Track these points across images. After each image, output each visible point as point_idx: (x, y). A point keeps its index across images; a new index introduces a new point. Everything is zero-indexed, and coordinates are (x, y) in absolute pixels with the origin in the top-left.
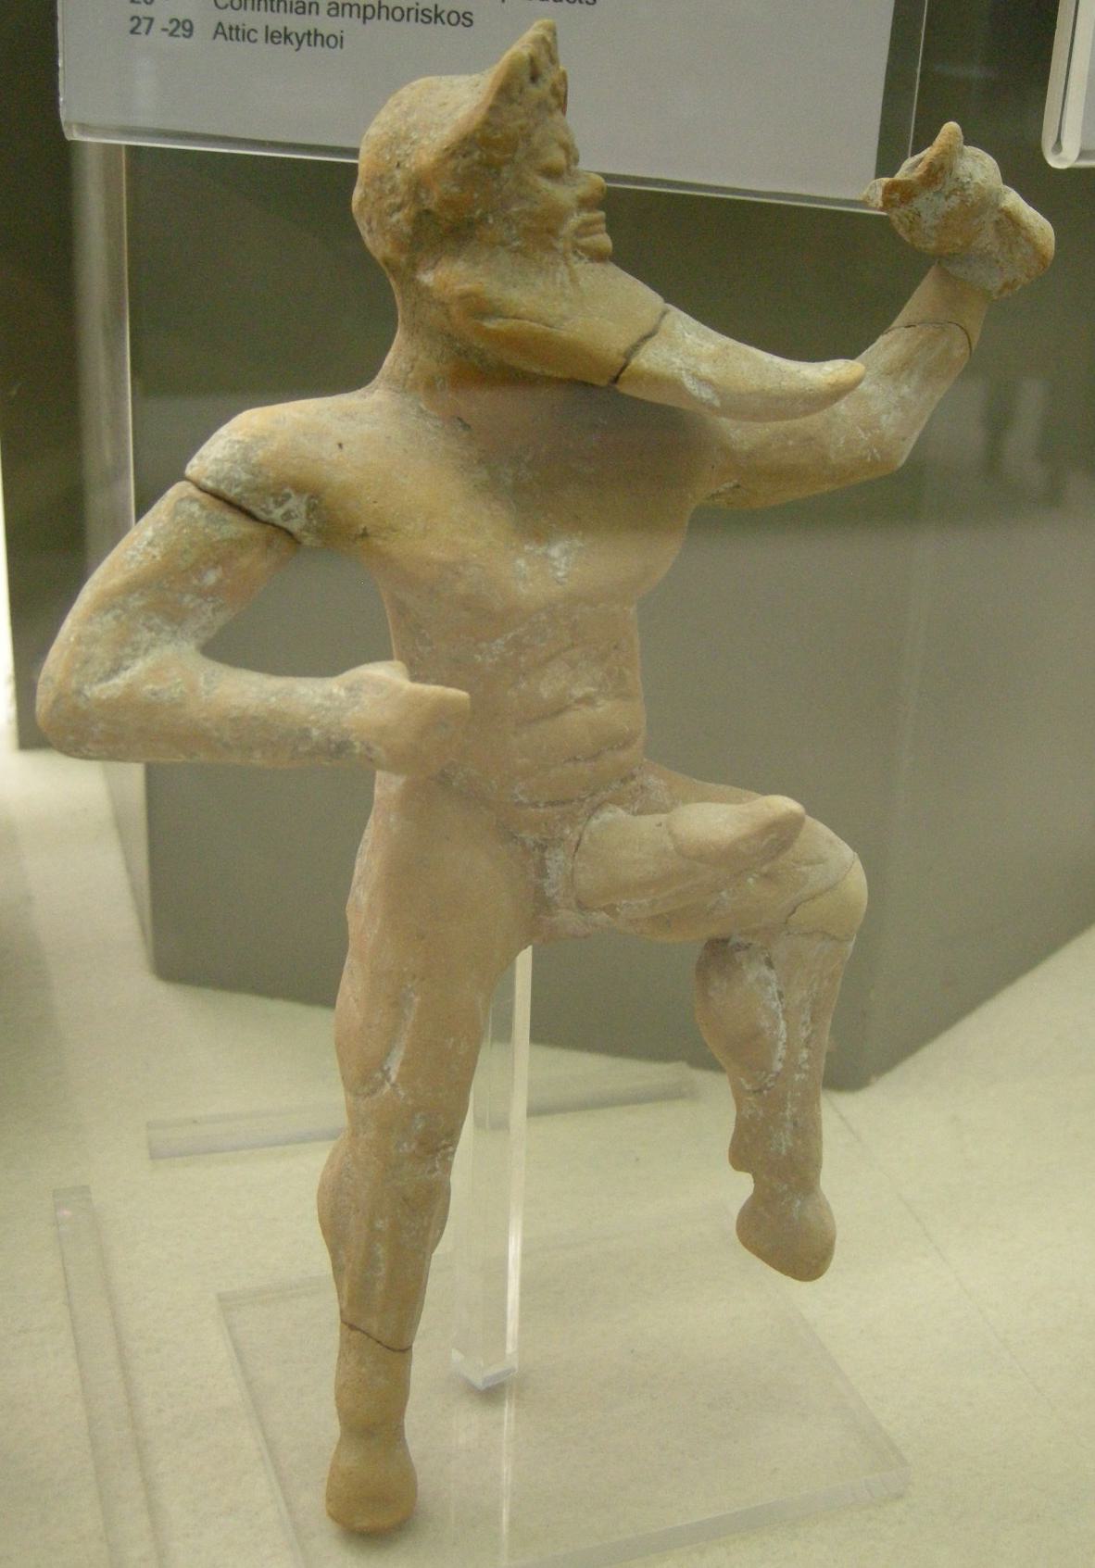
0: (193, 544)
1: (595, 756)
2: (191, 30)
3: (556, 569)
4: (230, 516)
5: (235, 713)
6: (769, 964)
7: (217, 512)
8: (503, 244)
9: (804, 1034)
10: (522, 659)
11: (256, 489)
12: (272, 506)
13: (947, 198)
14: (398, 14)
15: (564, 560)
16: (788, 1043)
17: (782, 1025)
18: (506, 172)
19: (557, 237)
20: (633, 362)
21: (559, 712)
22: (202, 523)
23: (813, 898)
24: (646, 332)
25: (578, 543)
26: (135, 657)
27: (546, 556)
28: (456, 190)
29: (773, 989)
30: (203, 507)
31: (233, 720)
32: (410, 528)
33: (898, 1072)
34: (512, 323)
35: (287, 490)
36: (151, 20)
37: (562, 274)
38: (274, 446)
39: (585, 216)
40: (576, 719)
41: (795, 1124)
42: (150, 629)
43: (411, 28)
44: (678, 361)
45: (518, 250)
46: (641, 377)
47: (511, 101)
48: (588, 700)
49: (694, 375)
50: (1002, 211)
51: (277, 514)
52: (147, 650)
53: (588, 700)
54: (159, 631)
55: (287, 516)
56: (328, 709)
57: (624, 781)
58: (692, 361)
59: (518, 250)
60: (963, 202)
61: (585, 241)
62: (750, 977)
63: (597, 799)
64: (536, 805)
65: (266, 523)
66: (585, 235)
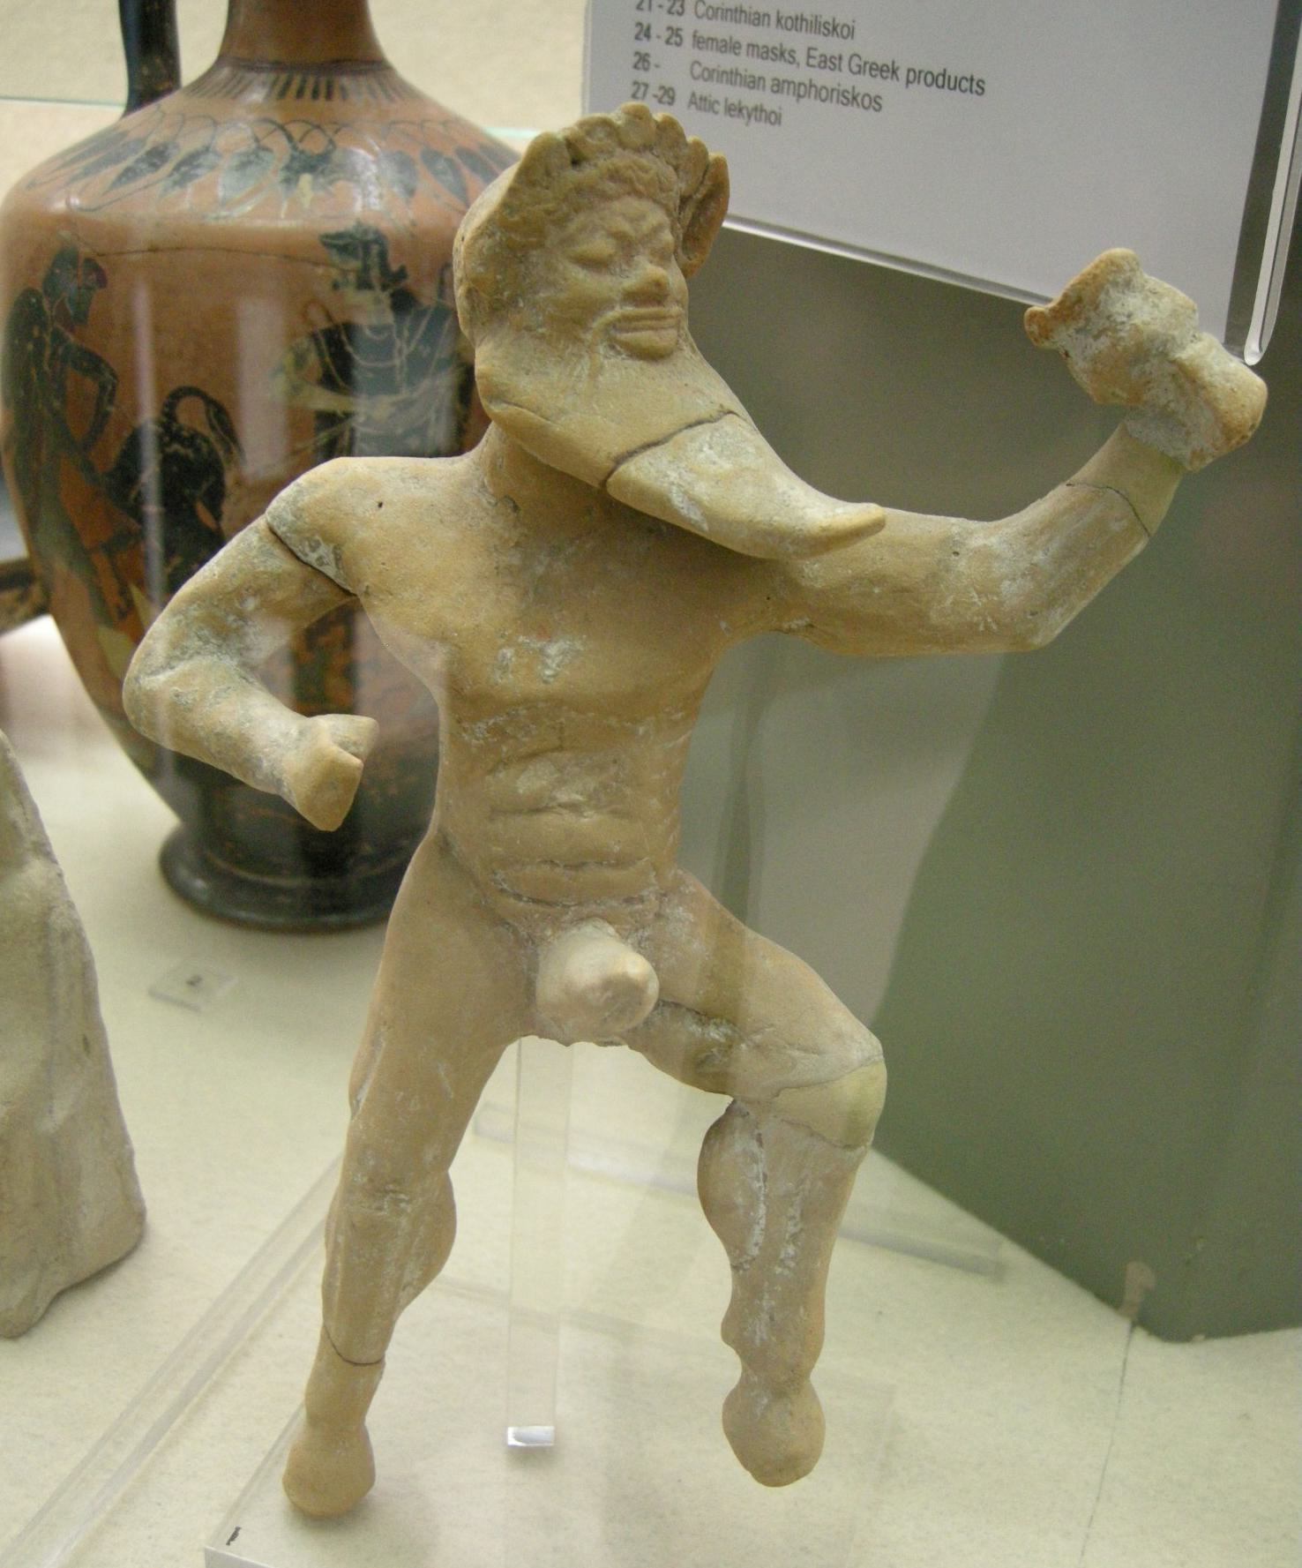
0: (240, 570)
1: (578, 866)
2: (673, 98)
3: (547, 666)
4: (277, 551)
5: (219, 729)
6: (759, 1140)
7: (268, 546)
8: (528, 329)
9: (792, 1229)
10: (505, 749)
11: (297, 531)
12: (307, 550)
13: (1096, 337)
14: (824, 94)
15: (557, 660)
16: (766, 1230)
17: (762, 1210)
18: (535, 255)
19: (586, 329)
20: (622, 468)
21: (537, 810)
22: (254, 553)
23: (799, 1087)
24: (653, 438)
25: (578, 646)
26: (181, 659)
27: (542, 651)
28: (481, 269)
29: (759, 1169)
30: (261, 539)
31: (217, 734)
32: (406, 595)
33: (1235, 1342)
34: (513, 409)
35: (317, 537)
36: (646, 86)
37: (584, 367)
38: (319, 494)
39: (630, 310)
40: (551, 823)
41: (772, 1319)
42: (200, 638)
43: (832, 107)
44: (673, 476)
45: (542, 337)
46: (624, 484)
47: (533, 184)
48: (574, 807)
49: (685, 493)
50: (1173, 362)
51: (312, 558)
52: (191, 657)
53: (574, 807)
54: (207, 642)
55: (320, 559)
56: (279, 746)
57: (629, 901)
58: (689, 477)
59: (542, 337)
60: (1114, 345)
61: (625, 336)
62: (738, 1148)
63: (585, 911)
64: (518, 897)
65: (306, 564)
66: (622, 330)
